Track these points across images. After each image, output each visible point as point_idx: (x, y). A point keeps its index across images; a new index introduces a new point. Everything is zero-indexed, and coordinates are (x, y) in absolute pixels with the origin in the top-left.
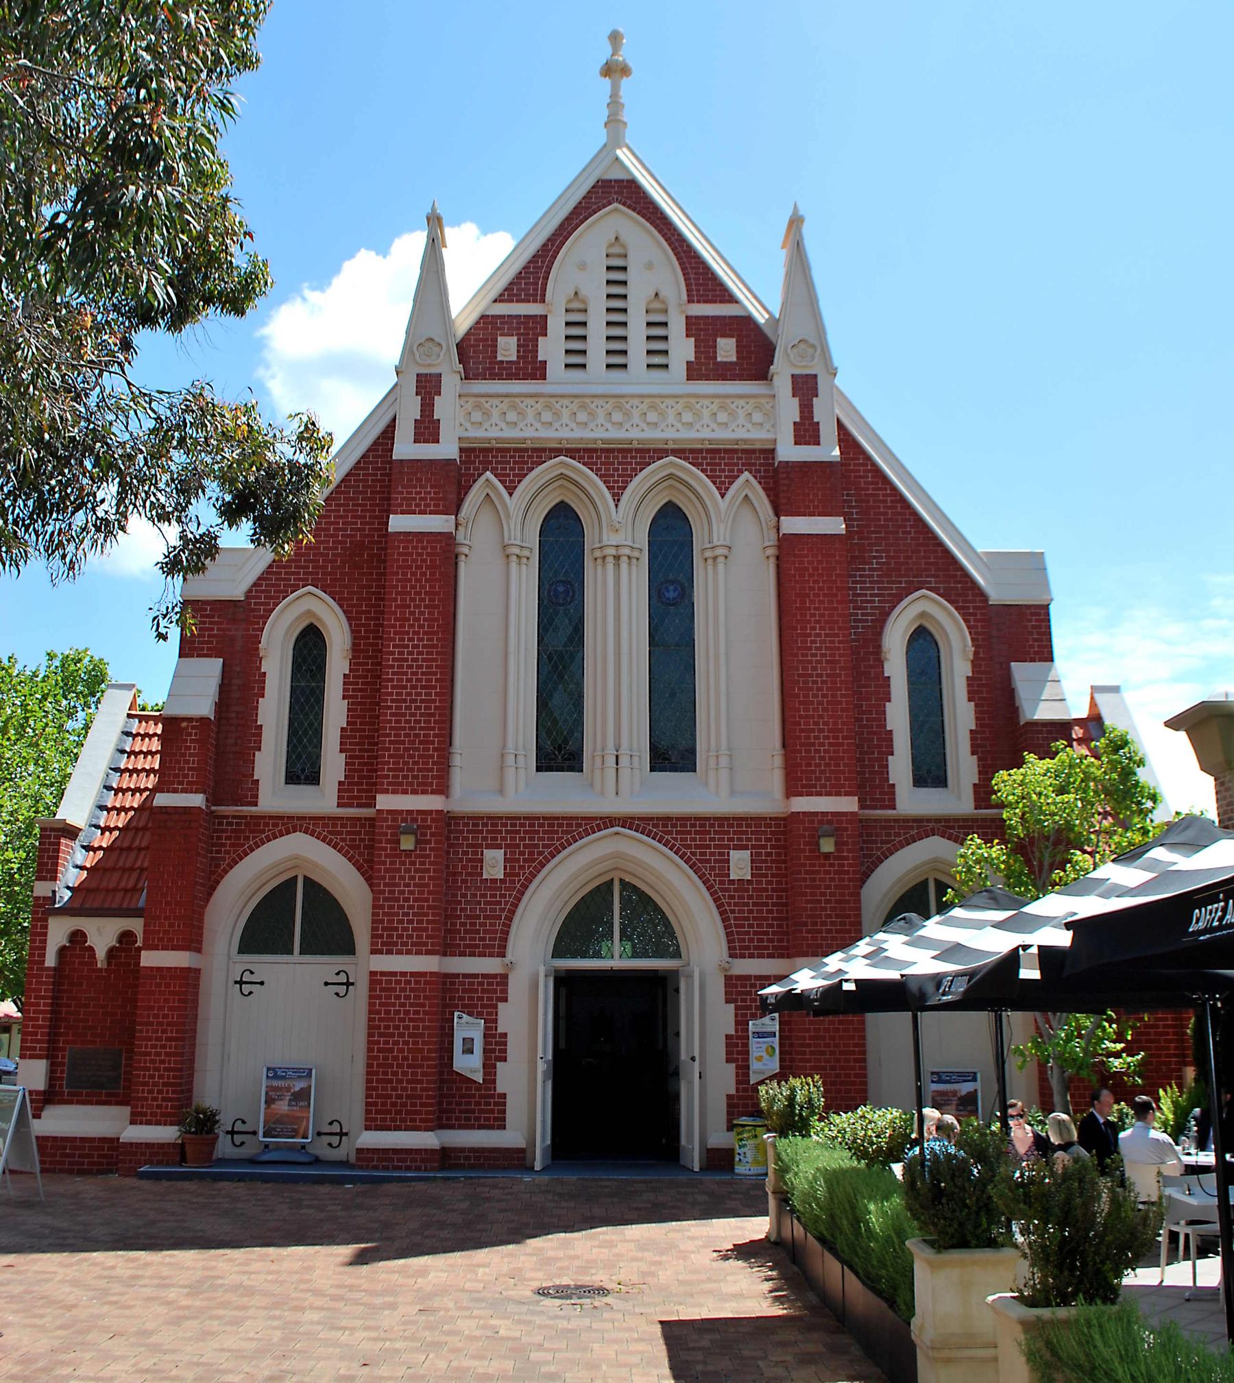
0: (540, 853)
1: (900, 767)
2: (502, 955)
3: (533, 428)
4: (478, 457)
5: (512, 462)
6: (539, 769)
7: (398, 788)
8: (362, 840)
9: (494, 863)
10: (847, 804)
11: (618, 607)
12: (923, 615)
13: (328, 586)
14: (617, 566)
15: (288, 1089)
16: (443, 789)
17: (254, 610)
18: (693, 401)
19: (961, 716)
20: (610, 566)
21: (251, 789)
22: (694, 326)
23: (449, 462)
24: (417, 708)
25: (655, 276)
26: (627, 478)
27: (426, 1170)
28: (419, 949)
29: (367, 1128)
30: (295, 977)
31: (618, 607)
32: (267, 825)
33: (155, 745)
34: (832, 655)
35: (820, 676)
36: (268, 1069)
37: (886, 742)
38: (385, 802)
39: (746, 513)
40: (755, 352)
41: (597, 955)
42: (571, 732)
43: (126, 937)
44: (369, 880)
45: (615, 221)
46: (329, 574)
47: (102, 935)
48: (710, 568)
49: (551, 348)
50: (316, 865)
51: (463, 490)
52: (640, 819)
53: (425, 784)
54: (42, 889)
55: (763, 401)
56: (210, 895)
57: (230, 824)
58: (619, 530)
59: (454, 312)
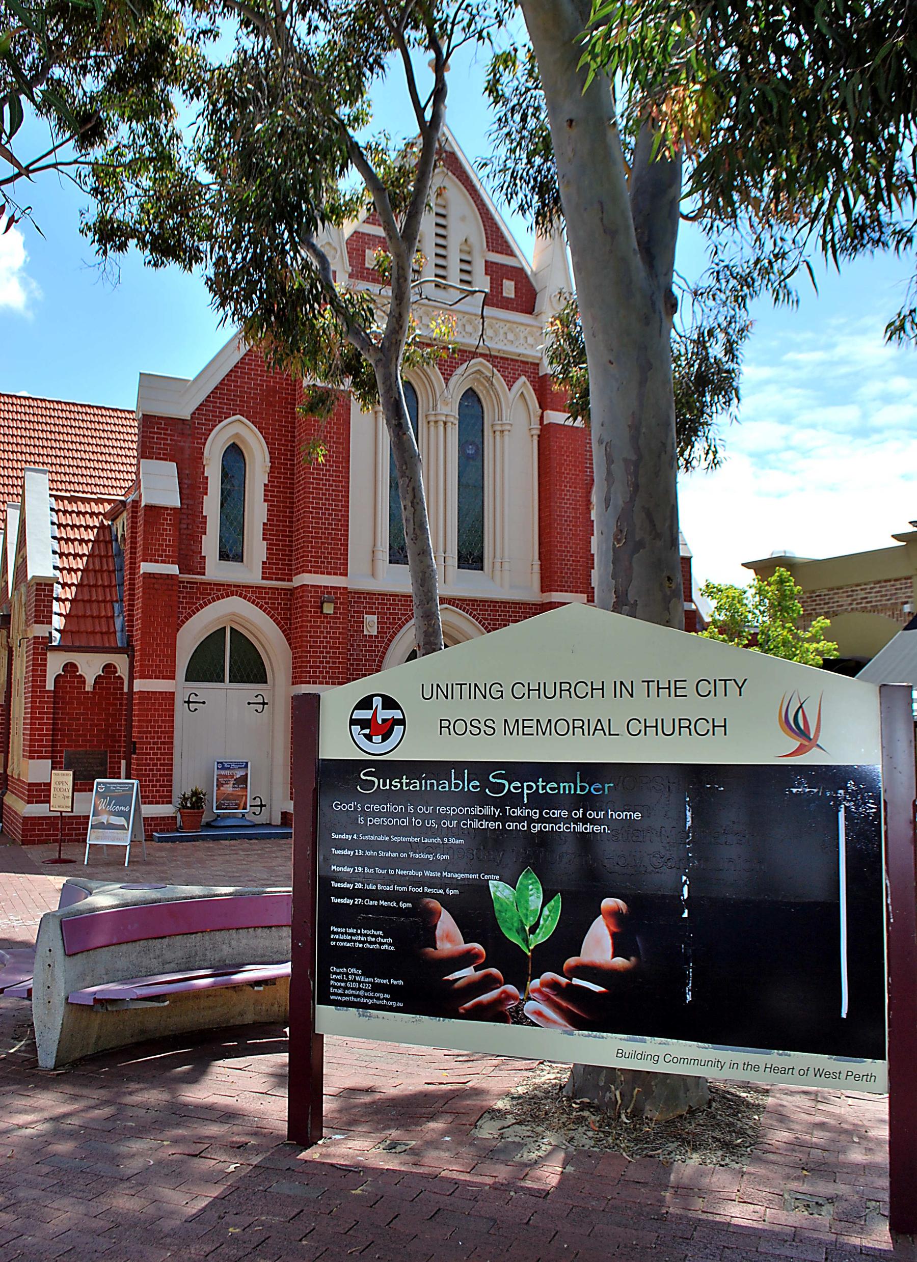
0: (400, 619)
1: (210, 544)
3: (503, 344)
8: (286, 608)
9: (371, 624)
12: (237, 435)
13: (251, 417)
15: (232, 776)
17: (198, 428)
18: (494, 322)
21: (200, 563)
22: (490, 267)
24: (330, 515)
27: (168, 831)
30: (226, 699)
32: (212, 589)
34: (575, 505)
35: (568, 517)
36: (218, 763)
39: (521, 404)
43: (109, 668)
46: (252, 407)
47: (90, 667)
48: (432, 429)
52: (459, 600)
53: (336, 568)
54: (40, 630)
55: (535, 330)
57: (185, 587)
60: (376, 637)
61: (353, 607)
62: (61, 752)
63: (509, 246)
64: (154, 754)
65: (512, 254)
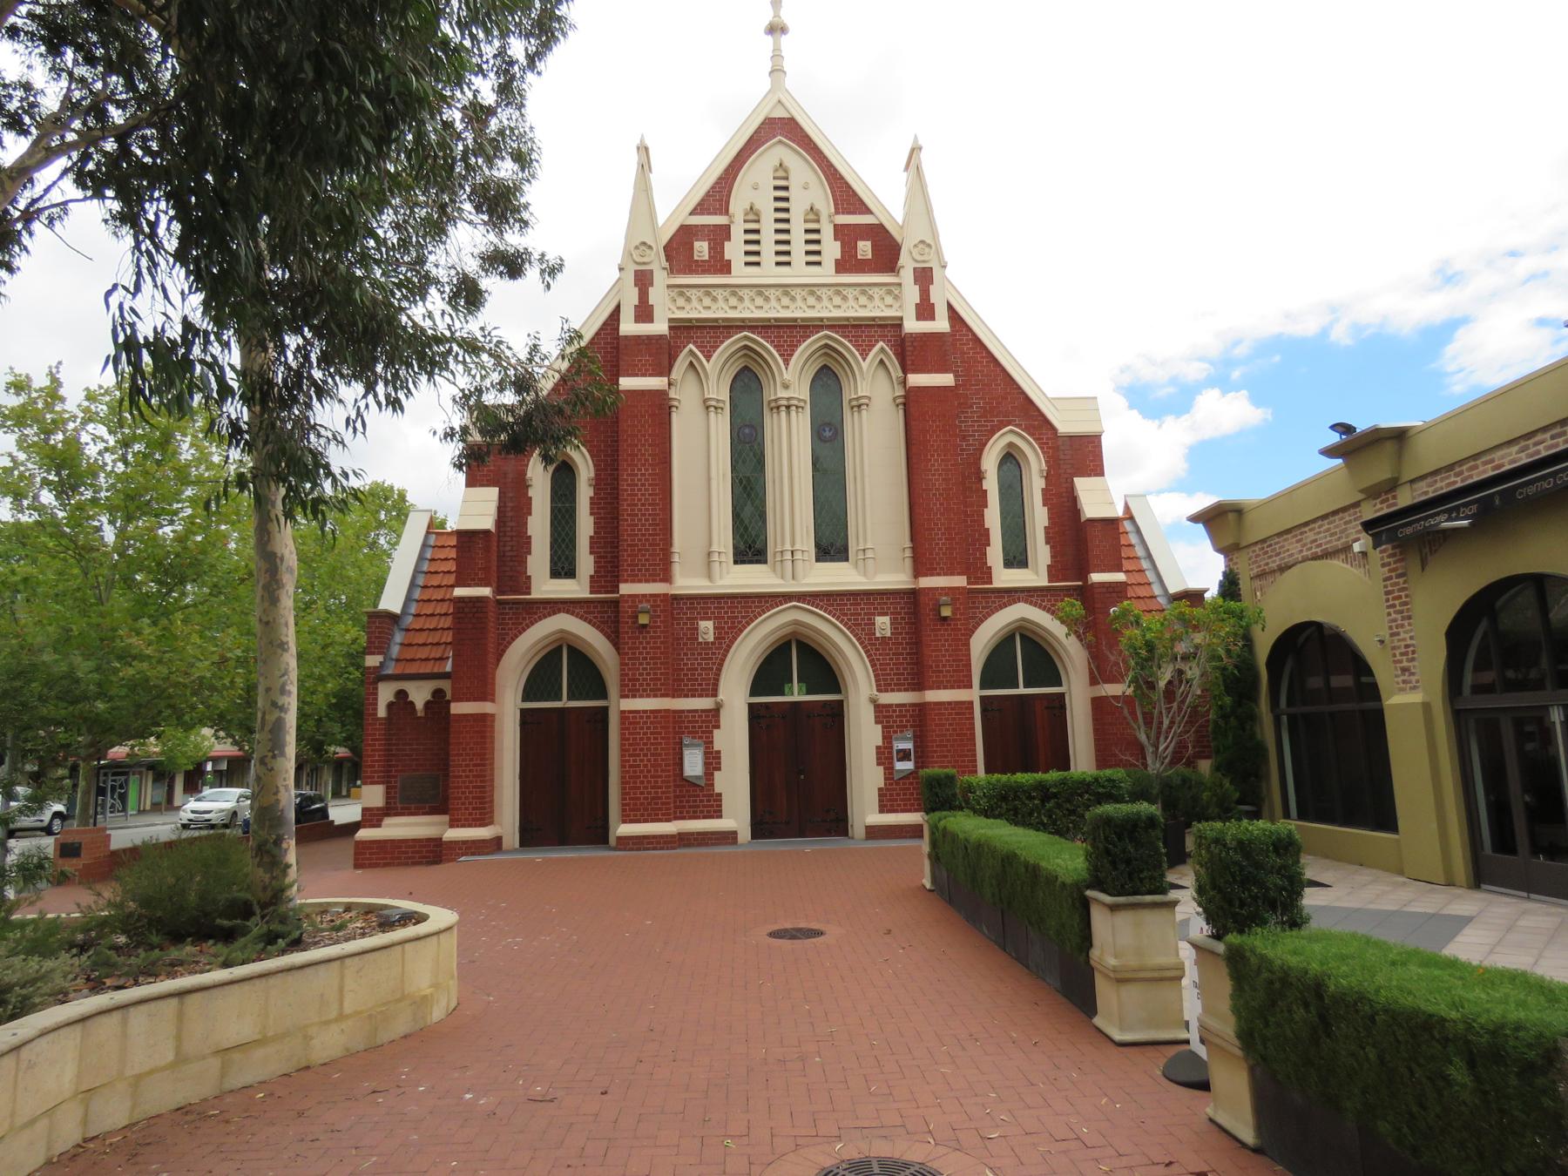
1: (995, 554)
2: (715, 695)
4: (684, 330)
5: (708, 333)
6: (736, 562)
7: (635, 579)
9: (707, 629)
10: (960, 581)
11: (790, 446)
12: (1011, 445)
14: (788, 413)
16: (667, 577)
19: (1038, 517)
20: (783, 414)
22: (840, 232)
23: (660, 338)
25: (809, 192)
26: (793, 347)
28: (655, 693)
29: (624, 822)
31: (790, 446)
33: (453, 554)
37: (985, 536)
38: (626, 589)
39: (881, 373)
40: (886, 252)
41: (783, 694)
42: (757, 536)
43: (438, 693)
44: (617, 649)
45: (777, 152)
49: (734, 250)
50: (590, 645)
51: (672, 359)
56: (499, 660)
58: (792, 379)
59: (661, 221)
65: (868, 211)
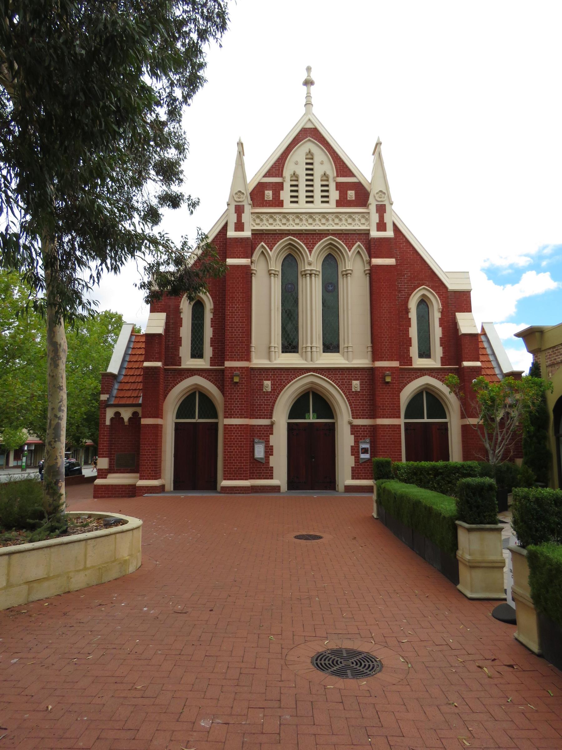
0: (284, 382)
9: (268, 384)
22: (340, 187)
35: (386, 317)
60: (270, 392)
61: (257, 377)
62: (114, 454)
63: (350, 170)
64: (148, 455)
65: (353, 175)
